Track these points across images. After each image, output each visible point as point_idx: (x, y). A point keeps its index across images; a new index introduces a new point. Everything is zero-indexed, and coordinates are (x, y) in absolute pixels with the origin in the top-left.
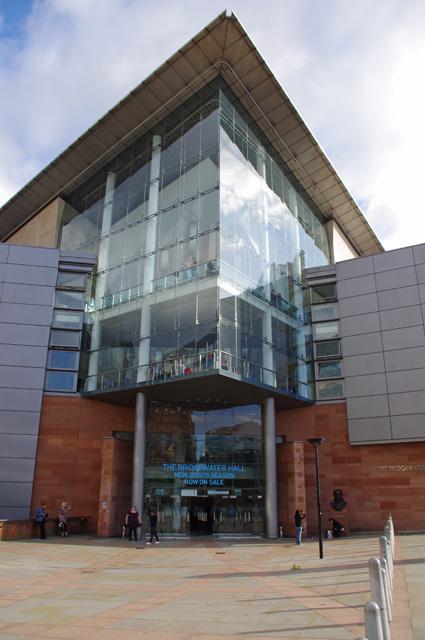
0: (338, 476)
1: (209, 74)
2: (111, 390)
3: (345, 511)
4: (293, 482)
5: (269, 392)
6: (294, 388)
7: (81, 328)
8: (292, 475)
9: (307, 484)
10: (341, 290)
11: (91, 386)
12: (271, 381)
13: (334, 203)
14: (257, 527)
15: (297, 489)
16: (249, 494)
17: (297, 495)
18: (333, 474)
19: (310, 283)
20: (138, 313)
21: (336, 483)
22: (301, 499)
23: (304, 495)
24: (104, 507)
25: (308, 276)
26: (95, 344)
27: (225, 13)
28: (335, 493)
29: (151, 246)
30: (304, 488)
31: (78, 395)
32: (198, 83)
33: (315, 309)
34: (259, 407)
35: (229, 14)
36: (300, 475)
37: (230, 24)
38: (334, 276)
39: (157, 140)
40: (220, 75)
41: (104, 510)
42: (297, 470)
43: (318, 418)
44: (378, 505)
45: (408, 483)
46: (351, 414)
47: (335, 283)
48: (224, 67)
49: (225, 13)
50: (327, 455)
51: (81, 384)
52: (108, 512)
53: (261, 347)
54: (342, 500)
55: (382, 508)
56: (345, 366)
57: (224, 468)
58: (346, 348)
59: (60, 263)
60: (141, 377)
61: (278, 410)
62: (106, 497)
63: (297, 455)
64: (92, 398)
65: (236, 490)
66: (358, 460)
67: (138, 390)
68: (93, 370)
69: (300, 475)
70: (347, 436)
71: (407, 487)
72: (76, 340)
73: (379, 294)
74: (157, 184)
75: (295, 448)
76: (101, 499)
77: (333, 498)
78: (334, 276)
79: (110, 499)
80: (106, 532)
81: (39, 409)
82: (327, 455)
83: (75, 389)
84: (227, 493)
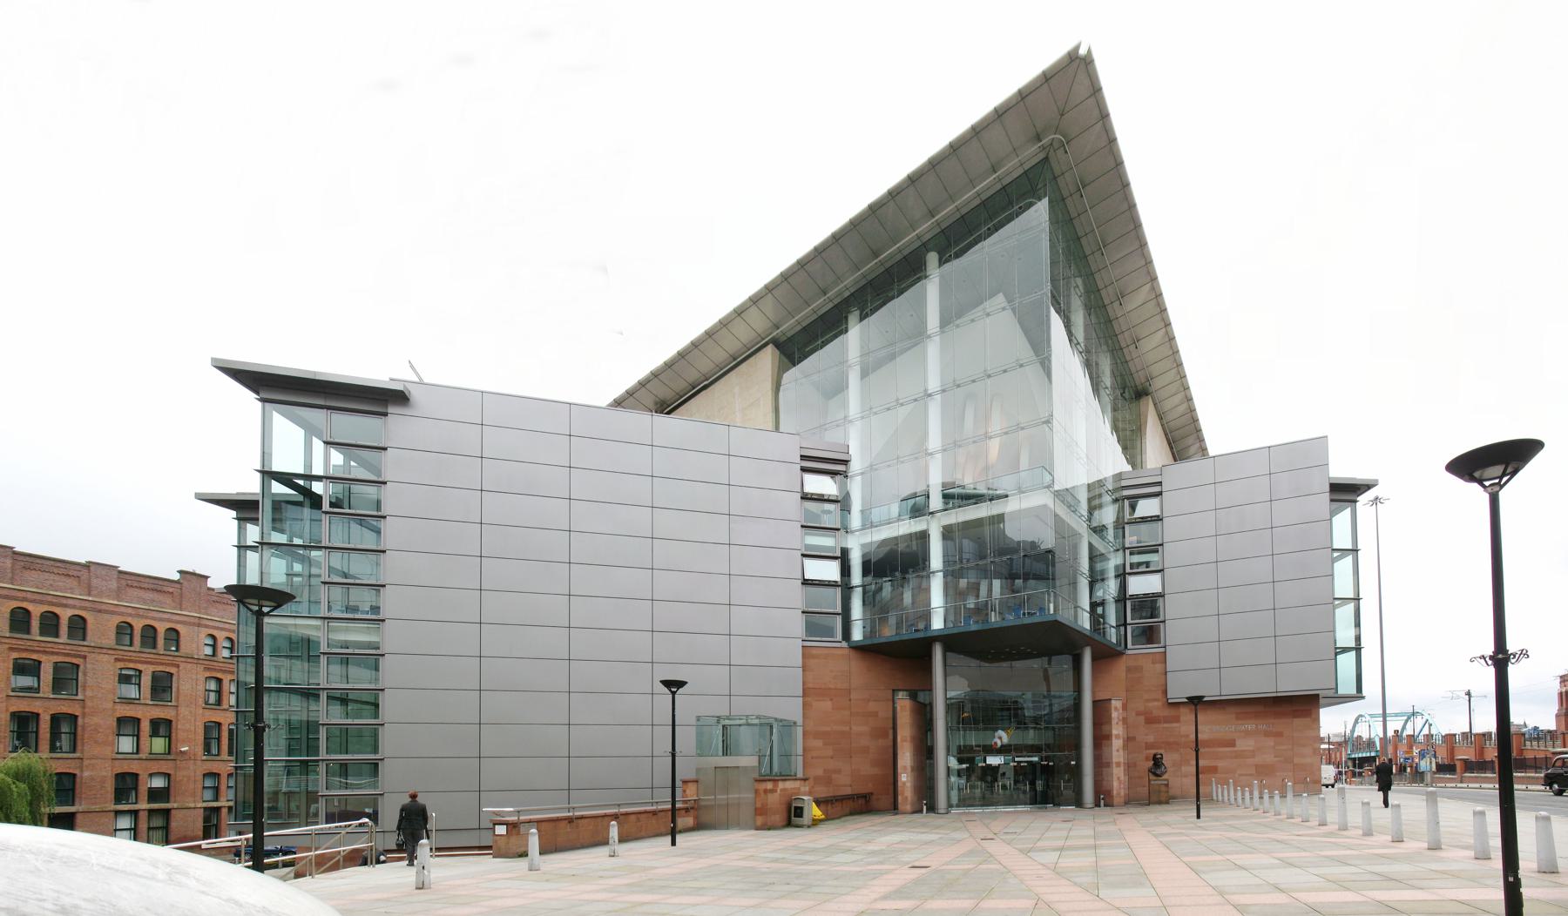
0: (1151, 739)
1: (1031, 154)
9: (1125, 747)
11: (857, 635)
12: (1085, 623)
13: (1155, 369)
14: (885, 801)
15: (1115, 753)
17: (1115, 760)
18: (1147, 735)
20: (923, 536)
21: (1148, 746)
22: (1118, 764)
25: (1124, 483)
26: (857, 578)
27: (1077, 48)
28: (207, 728)
29: (934, 441)
31: (844, 644)
32: (1012, 168)
34: (1069, 658)
35: (1082, 51)
36: (1117, 737)
37: (1082, 66)
39: (932, 258)
40: (1046, 158)
42: (1114, 732)
43: (1129, 670)
46: (1171, 664)
48: (1056, 145)
49: (1077, 48)
50: (1138, 714)
60: (937, 623)
61: (1094, 659)
63: (1114, 715)
64: (860, 649)
66: (1177, 719)
69: (1117, 737)
70: (1165, 692)
74: (858, 368)
78: (1160, 483)
80: (909, 808)
82: (1138, 714)
83: (839, 637)
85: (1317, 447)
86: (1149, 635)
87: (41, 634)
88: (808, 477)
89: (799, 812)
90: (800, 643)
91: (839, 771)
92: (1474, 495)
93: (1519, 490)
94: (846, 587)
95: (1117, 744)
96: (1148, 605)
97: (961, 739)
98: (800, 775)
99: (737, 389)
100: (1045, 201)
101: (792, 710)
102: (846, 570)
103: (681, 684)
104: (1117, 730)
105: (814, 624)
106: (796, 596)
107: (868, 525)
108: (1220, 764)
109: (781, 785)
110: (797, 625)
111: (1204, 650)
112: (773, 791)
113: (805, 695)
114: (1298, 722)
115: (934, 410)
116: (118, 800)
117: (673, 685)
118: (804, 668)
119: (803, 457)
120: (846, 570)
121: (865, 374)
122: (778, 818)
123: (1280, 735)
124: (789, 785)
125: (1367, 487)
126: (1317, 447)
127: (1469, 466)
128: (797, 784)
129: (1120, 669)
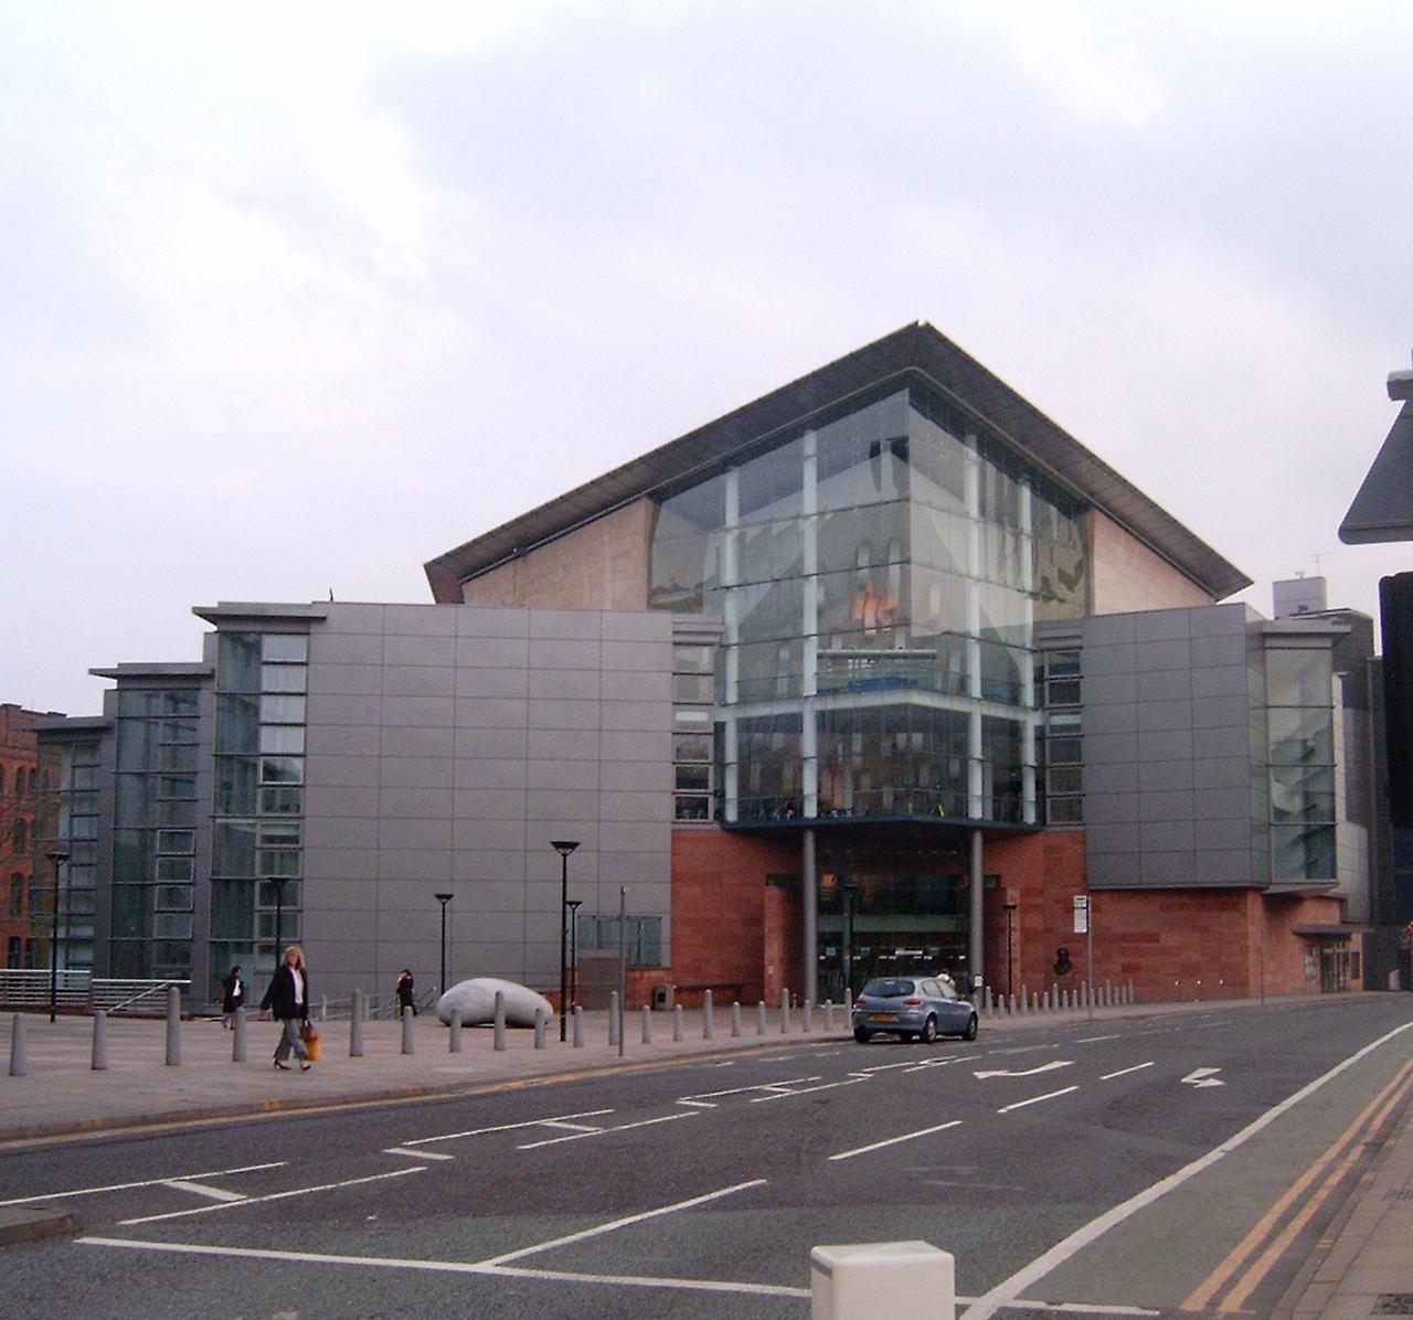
3: (1069, 975)
7: (712, 730)
11: (731, 815)
16: (270, 1244)
19: (1046, 644)
24: (771, 972)
25: (1046, 634)
27: (917, 323)
38: (1079, 637)
41: (771, 976)
44: (1119, 967)
45: (1158, 941)
47: (1081, 648)
50: (1056, 902)
51: (720, 814)
52: (775, 978)
53: (1033, 531)
54: (1068, 961)
55: (1124, 970)
59: (675, 632)
61: (985, 842)
62: (772, 961)
64: (732, 830)
65: (932, 949)
67: (809, 827)
70: (1085, 878)
75: (1009, 897)
76: (766, 962)
77: (1057, 958)
78: (1079, 637)
79: (777, 961)
84: (921, 952)
86: (1072, 811)
87: (262, 904)
89: (662, 998)
91: (708, 961)
92: (557, 856)
93: (573, 857)
97: (833, 924)
98: (666, 963)
99: (606, 538)
103: (573, 845)
107: (743, 701)
108: (1143, 961)
109: (646, 974)
110: (664, 806)
114: (1224, 916)
116: (1071, 801)
117: (565, 846)
118: (674, 853)
119: (675, 632)
121: (820, 477)
123: (1205, 929)
124: (654, 974)
125: (577, 844)
127: (439, 897)
128: (661, 974)
129: (1034, 850)
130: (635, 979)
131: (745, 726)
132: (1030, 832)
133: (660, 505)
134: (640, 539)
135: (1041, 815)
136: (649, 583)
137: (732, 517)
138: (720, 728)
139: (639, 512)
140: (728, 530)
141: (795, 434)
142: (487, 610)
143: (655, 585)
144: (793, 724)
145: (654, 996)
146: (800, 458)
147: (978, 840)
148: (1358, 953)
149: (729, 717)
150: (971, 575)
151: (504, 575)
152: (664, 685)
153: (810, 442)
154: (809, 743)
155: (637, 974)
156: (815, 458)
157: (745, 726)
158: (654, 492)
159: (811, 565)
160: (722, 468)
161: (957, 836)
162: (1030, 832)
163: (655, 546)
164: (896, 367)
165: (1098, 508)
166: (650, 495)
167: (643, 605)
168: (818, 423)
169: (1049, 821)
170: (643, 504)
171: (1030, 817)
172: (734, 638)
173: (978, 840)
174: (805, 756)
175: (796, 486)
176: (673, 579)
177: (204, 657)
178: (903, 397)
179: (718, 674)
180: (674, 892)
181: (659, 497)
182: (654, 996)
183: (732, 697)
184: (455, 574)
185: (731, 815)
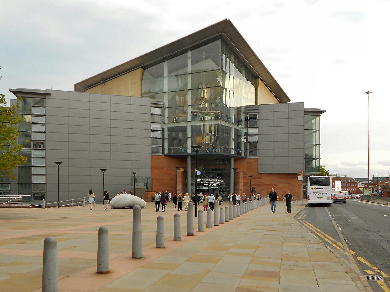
2: (178, 154)
4: (239, 185)
5: (232, 156)
6: (240, 154)
8: (239, 182)
9: (244, 185)
10: (260, 116)
11: (166, 152)
12: (232, 153)
15: (240, 187)
19: (248, 111)
22: (241, 190)
23: (242, 189)
29: (189, 102)
30: (242, 187)
31: (163, 155)
33: (160, 113)
36: (241, 182)
42: (240, 181)
43: (248, 163)
44: (266, 192)
45: (277, 186)
47: (258, 113)
51: (163, 152)
56: (260, 153)
57: (216, 180)
58: (259, 146)
61: (235, 160)
64: (167, 156)
66: (261, 178)
68: (166, 146)
69: (241, 182)
70: (258, 170)
71: (277, 187)
72: (159, 135)
73: (68, 166)
75: (240, 174)
81: (150, 160)
83: (161, 153)
85: (302, 103)
88: (152, 109)
90: (150, 154)
94: (163, 139)
95: (241, 184)
96: (254, 145)
100: (220, 40)
101: (147, 173)
102: (163, 135)
104: (241, 181)
105: (154, 147)
106: (149, 142)
110: (149, 149)
111: (270, 159)
112: (149, 194)
113: (151, 168)
115: (189, 78)
117: (103, 170)
118: (151, 162)
120: (163, 135)
122: (150, 200)
126: (302, 103)
127: (102, 170)
129: (245, 163)
130: (148, 194)
131: (170, 129)
132: (243, 159)
133: (144, 70)
134: (139, 79)
135: (246, 155)
136: (142, 91)
137: (166, 74)
138: (163, 130)
139: (139, 71)
140: (165, 77)
141: (185, 52)
142: (82, 95)
143: (143, 92)
144: (184, 129)
145: (152, 199)
146: (187, 58)
147: (233, 160)
148: (277, 186)
149: (166, 127)
150: (239, 93)
151: (99, 88)
152: (148, 117)
153: (189, 54)
154: (189, 134)
155: (149, 193)
156: (191, 58)
157: (170, 129)
158: (142, 67)
159: (189, 87)
160: (163, 60)
161: (227, 159)
162: (243, 159)
163: (143, 81)
164: (218, 32)
165: (27, 97)
166: (142, 67)
167: (140, 96)
168: (192, 48)
169: (248, 156)
170: (140, 70)
171: (243, 155)
172: (166, 106)
173: (189, 159)
174: (165, 138)
175: (185, 66)
176: (149, 90)
177: (11, 105)
178: (218, 43)
179: (162, 115)
180: (152, 171)
181: (144, 68)
182: (152, 199)
183: (166, 121)
184: (85, 86)
185: (166, 152)
